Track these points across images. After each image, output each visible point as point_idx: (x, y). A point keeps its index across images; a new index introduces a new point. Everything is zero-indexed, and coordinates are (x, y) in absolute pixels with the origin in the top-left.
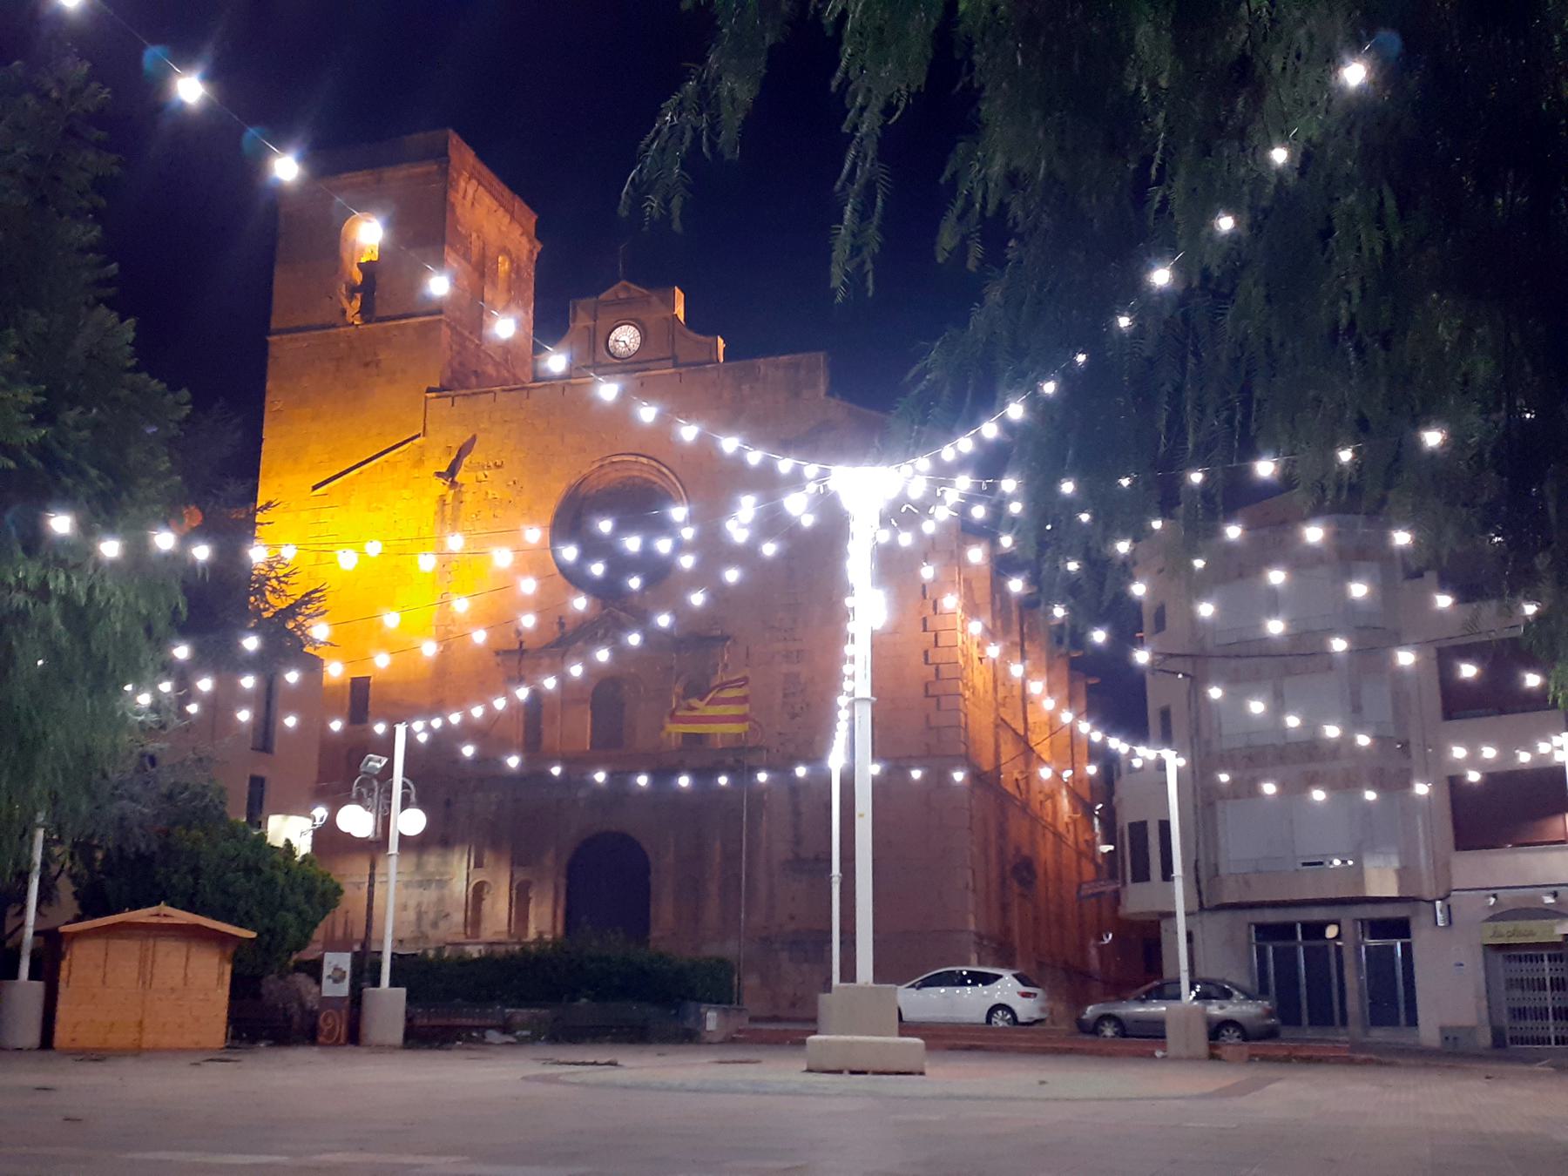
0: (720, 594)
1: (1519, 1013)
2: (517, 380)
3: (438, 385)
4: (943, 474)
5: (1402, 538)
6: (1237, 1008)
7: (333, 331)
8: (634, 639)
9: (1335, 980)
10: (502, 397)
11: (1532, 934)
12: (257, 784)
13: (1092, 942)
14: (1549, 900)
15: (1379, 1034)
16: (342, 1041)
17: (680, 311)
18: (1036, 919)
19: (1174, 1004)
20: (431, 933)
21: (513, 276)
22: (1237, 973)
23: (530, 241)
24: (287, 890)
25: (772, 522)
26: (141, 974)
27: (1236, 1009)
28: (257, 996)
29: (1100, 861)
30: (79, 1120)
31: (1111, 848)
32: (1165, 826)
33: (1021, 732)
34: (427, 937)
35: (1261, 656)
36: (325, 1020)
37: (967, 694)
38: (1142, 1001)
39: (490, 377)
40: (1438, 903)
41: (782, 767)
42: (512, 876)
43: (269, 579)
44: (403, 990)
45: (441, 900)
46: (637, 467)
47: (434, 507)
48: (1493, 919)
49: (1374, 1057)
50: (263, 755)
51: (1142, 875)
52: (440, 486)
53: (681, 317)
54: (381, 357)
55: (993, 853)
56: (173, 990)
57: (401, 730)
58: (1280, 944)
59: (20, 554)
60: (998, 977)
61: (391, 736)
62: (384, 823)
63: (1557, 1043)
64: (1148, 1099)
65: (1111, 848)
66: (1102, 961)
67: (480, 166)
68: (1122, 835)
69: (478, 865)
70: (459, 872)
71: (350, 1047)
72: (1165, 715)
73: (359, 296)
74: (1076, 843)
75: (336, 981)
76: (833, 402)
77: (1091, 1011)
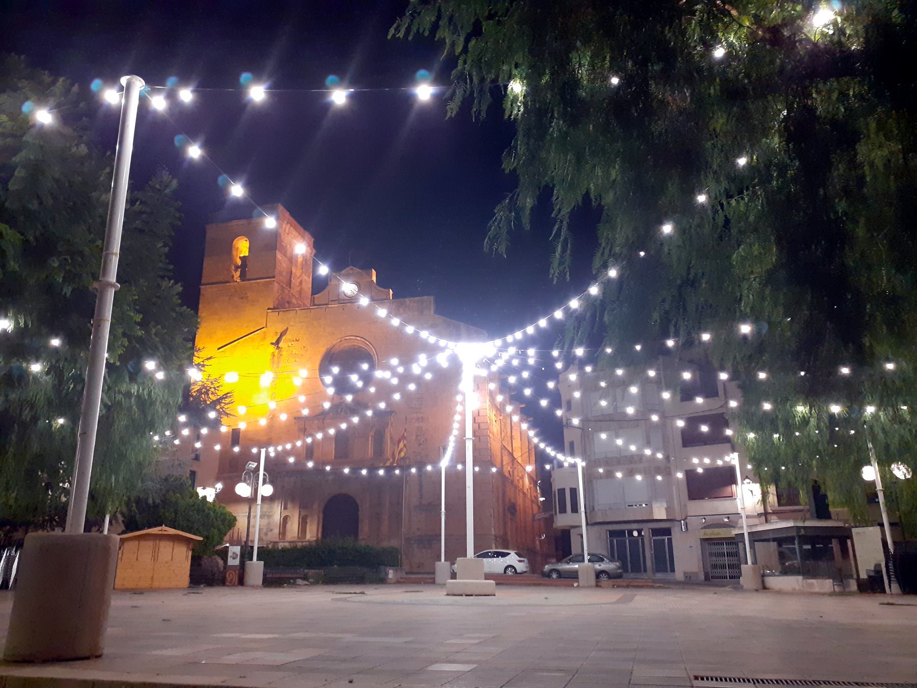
0: (406, 395)
1: (715, 566)
2: (304, 305)
3: (272, 307)
4: (505, 346)
5: (687, 376)
6: (605, 565)
7: (228, 284)
8: (369, 413)
9: (641, 555)
10: (299, 312)
11: (719, 534)
12: (193, 474)
13: (537, 538)
14: (726, 520)
15: (659, 576)
16: (236, 584)
17: (374, 278)
18: (516, 528)
19: (582, 564)
20: (264, 538)
21: (304, 263)
22: (602, 551)
23: (311, 249)
24: (215, 520)
25: (432, 367)
26: (153, 556)
27: (606, 566)
28: (200, 565)
29: (539, 504)
30: (169, 620)
31: (544, 499)
32: (574, 492)
33: (511, 451)
34: (263, 539)
35: (610, 421)
36: (229, 575)
37: (491, 435)
38: (568, 563)
39: (294, 304)
40: (682, 521)
41: (421, 466)
42: (300, 512)
43: (211, 388)
44: (263, 562)
45: (269, 524)
46: (356, 341)
47: (270, 357)
48: (705, 528)
49: (662, 585)
50: (195, 461)
51: (563, 510)
52: (272, 349)
53: (375, 281)
54: (248, 295)
55: (500, 501)
56: (167, 562)
57: (263, 451)
58: (619, 539)
59: (127, 380)
60: (509, 554)
61: (259, 453)
62: (256, 491)
63: (730, 578)
64: (913, 605)
65: (544, 499)
66: (541, 546)
67: (291, 218)
68: (555, 495)
69: (285, 508)
70: (277, 512)
71: (240, 587)
72: (572, 445)
73: (239, 270)
74: (531, 497)
75: (234, 558)
76: (437, 316)
77: (547, 568)
